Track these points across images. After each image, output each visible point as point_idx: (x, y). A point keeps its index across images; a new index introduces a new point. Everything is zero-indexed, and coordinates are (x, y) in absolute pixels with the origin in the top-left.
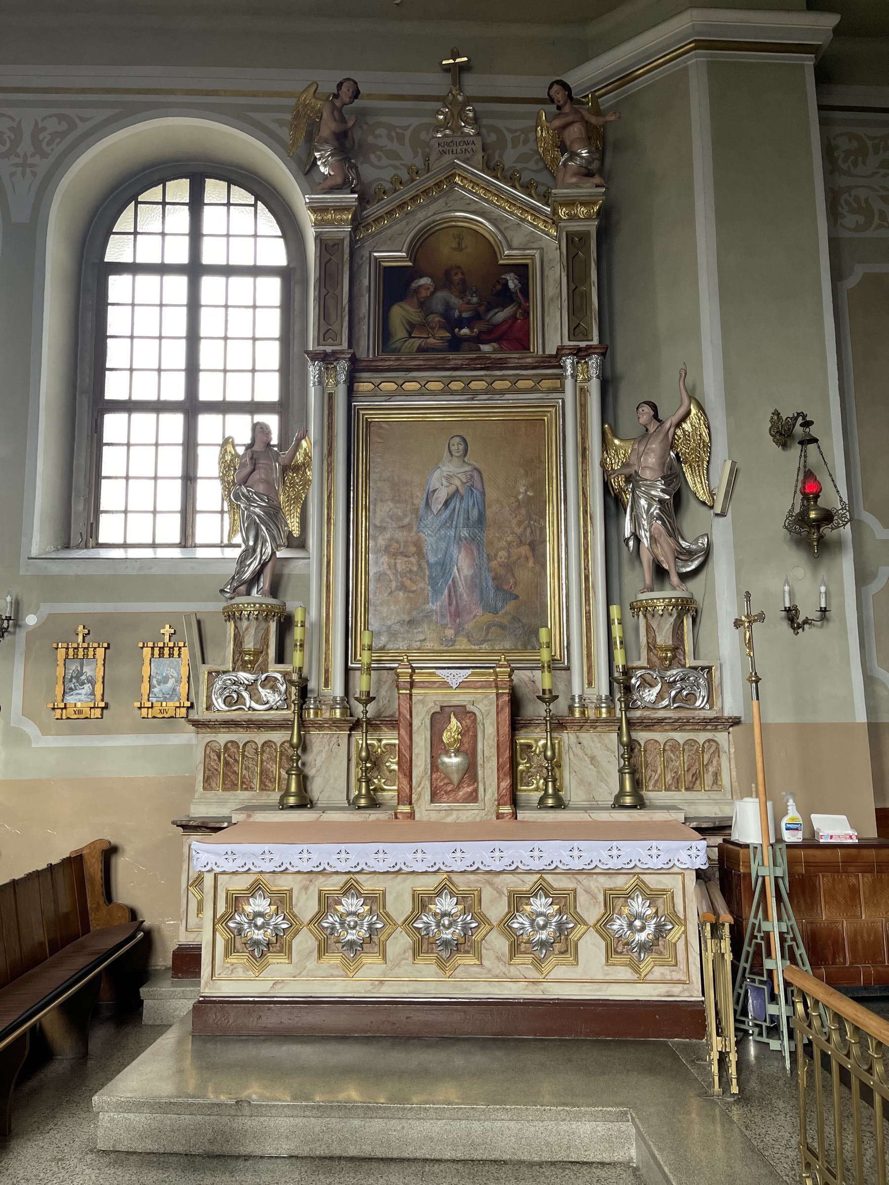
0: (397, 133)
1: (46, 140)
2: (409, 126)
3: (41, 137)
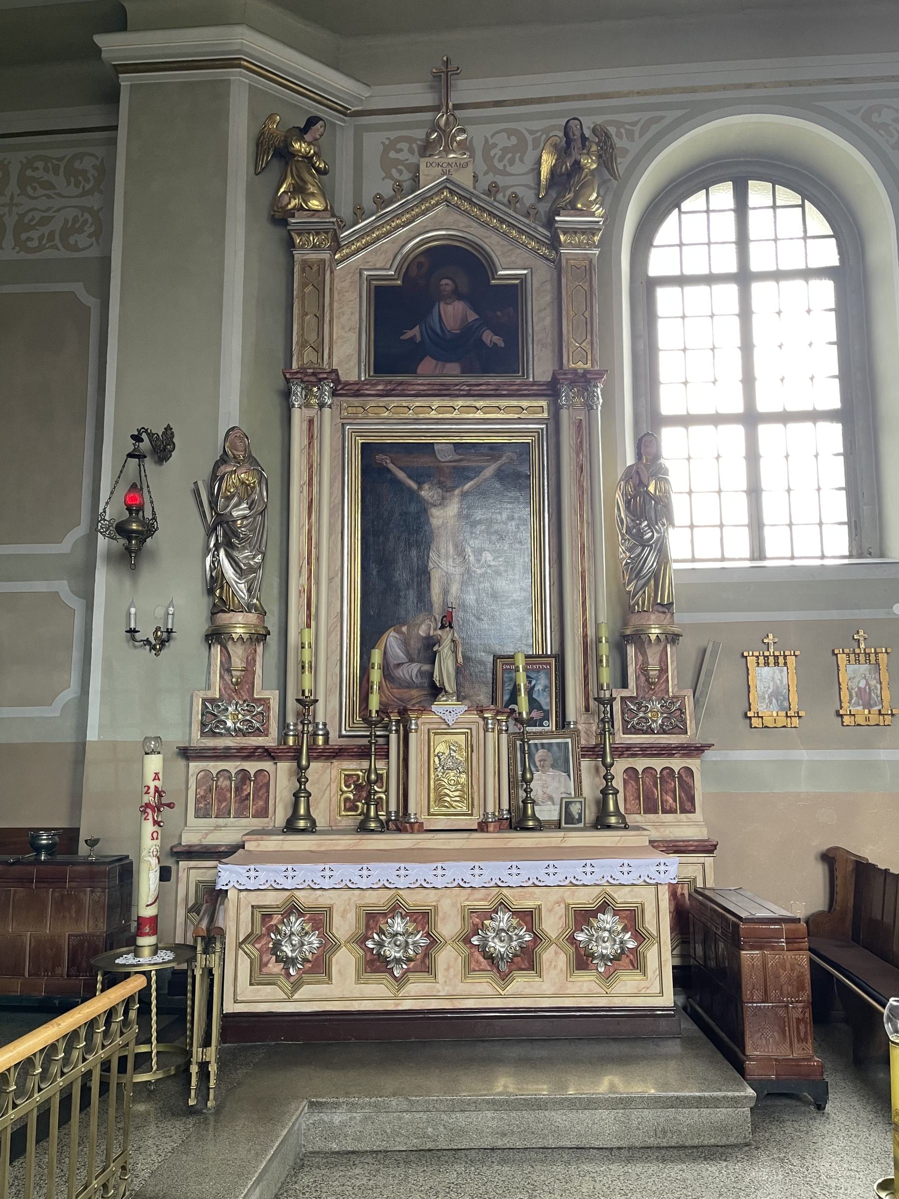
0: (625, 129)
1: (497, 156)
2: (637, 122)
3: (492, 153)
